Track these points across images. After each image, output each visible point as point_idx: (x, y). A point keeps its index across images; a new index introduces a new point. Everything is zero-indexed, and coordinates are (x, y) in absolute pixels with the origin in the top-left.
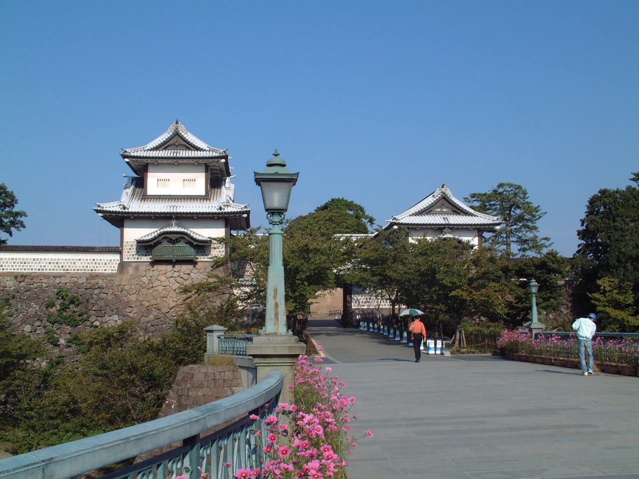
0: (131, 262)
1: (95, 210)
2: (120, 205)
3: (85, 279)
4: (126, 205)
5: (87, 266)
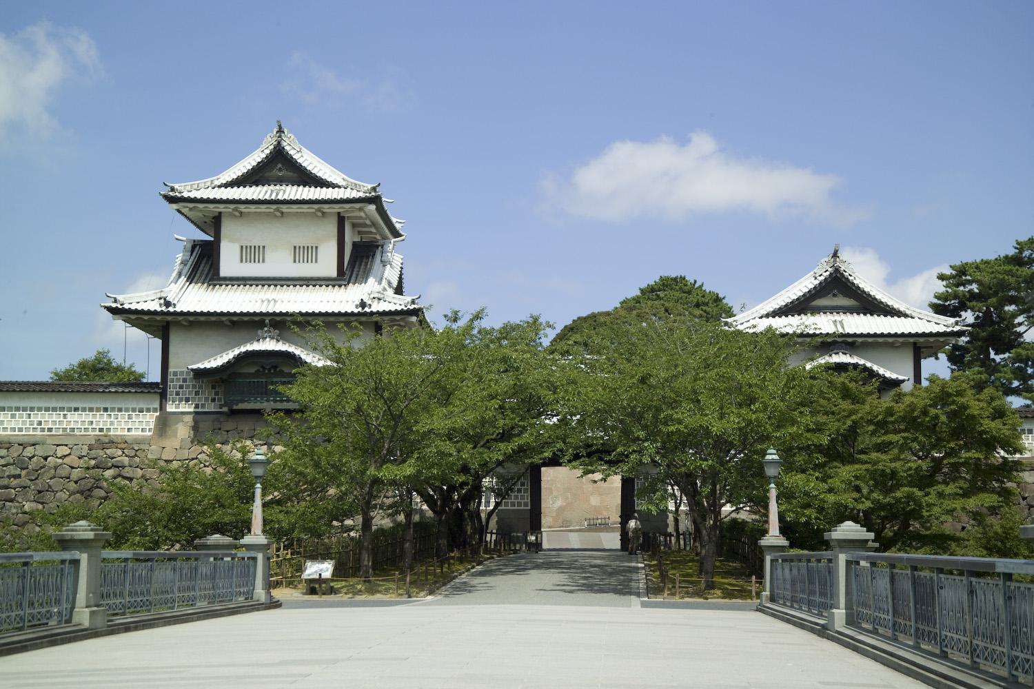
0: (183, 413)
1: (105, 307)
2: (160, 299)
3: (86, 448)
5: (92, 422)
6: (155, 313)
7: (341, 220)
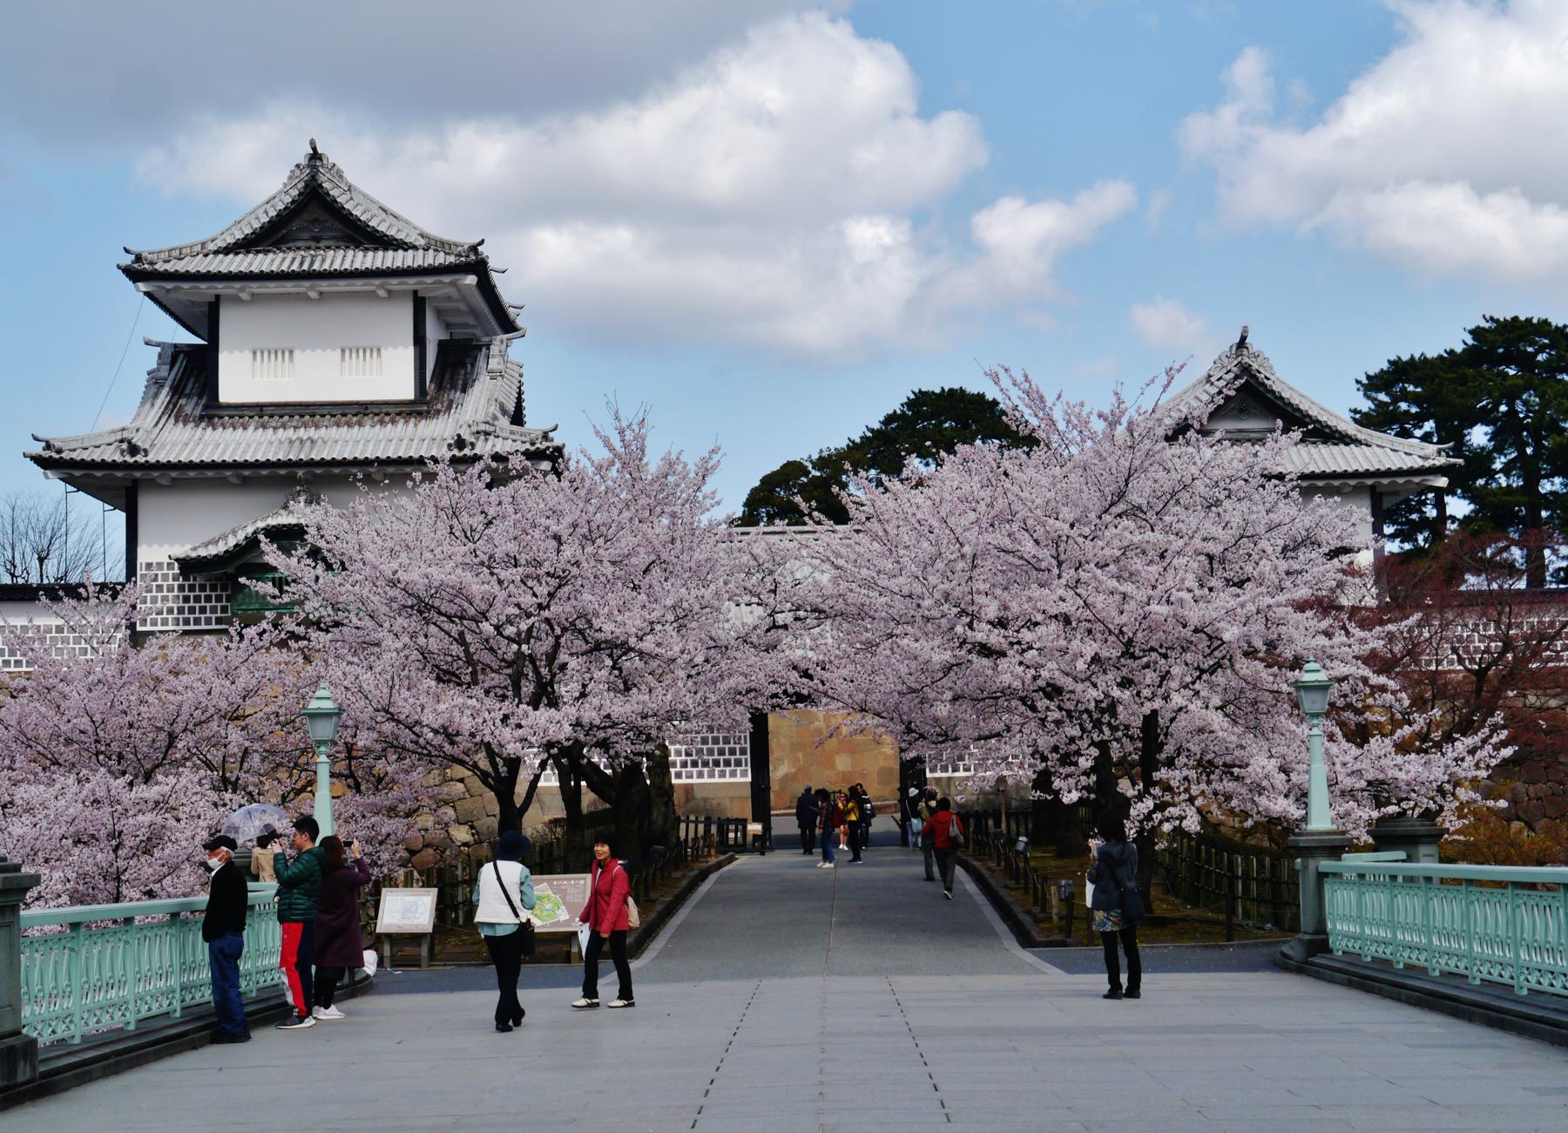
2: (122, 441)
4: (138, 440)
6: (114, 465)
7: (419, 305)
